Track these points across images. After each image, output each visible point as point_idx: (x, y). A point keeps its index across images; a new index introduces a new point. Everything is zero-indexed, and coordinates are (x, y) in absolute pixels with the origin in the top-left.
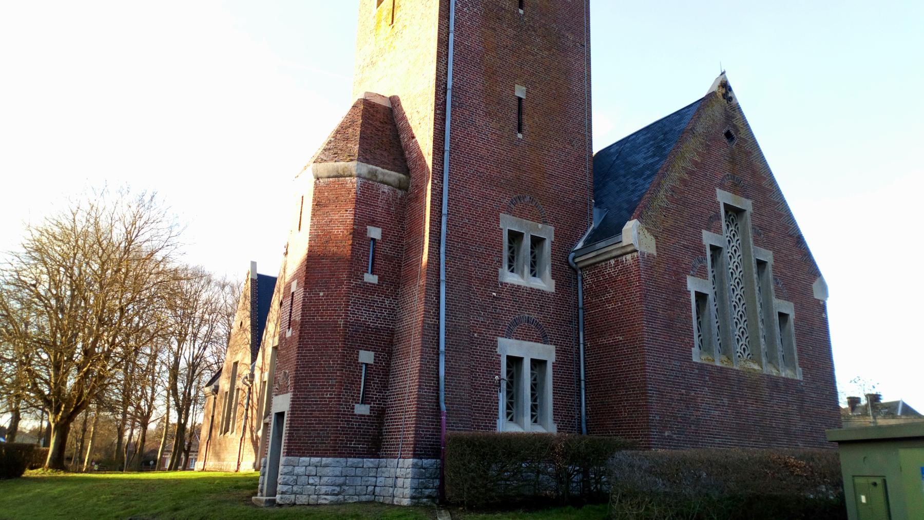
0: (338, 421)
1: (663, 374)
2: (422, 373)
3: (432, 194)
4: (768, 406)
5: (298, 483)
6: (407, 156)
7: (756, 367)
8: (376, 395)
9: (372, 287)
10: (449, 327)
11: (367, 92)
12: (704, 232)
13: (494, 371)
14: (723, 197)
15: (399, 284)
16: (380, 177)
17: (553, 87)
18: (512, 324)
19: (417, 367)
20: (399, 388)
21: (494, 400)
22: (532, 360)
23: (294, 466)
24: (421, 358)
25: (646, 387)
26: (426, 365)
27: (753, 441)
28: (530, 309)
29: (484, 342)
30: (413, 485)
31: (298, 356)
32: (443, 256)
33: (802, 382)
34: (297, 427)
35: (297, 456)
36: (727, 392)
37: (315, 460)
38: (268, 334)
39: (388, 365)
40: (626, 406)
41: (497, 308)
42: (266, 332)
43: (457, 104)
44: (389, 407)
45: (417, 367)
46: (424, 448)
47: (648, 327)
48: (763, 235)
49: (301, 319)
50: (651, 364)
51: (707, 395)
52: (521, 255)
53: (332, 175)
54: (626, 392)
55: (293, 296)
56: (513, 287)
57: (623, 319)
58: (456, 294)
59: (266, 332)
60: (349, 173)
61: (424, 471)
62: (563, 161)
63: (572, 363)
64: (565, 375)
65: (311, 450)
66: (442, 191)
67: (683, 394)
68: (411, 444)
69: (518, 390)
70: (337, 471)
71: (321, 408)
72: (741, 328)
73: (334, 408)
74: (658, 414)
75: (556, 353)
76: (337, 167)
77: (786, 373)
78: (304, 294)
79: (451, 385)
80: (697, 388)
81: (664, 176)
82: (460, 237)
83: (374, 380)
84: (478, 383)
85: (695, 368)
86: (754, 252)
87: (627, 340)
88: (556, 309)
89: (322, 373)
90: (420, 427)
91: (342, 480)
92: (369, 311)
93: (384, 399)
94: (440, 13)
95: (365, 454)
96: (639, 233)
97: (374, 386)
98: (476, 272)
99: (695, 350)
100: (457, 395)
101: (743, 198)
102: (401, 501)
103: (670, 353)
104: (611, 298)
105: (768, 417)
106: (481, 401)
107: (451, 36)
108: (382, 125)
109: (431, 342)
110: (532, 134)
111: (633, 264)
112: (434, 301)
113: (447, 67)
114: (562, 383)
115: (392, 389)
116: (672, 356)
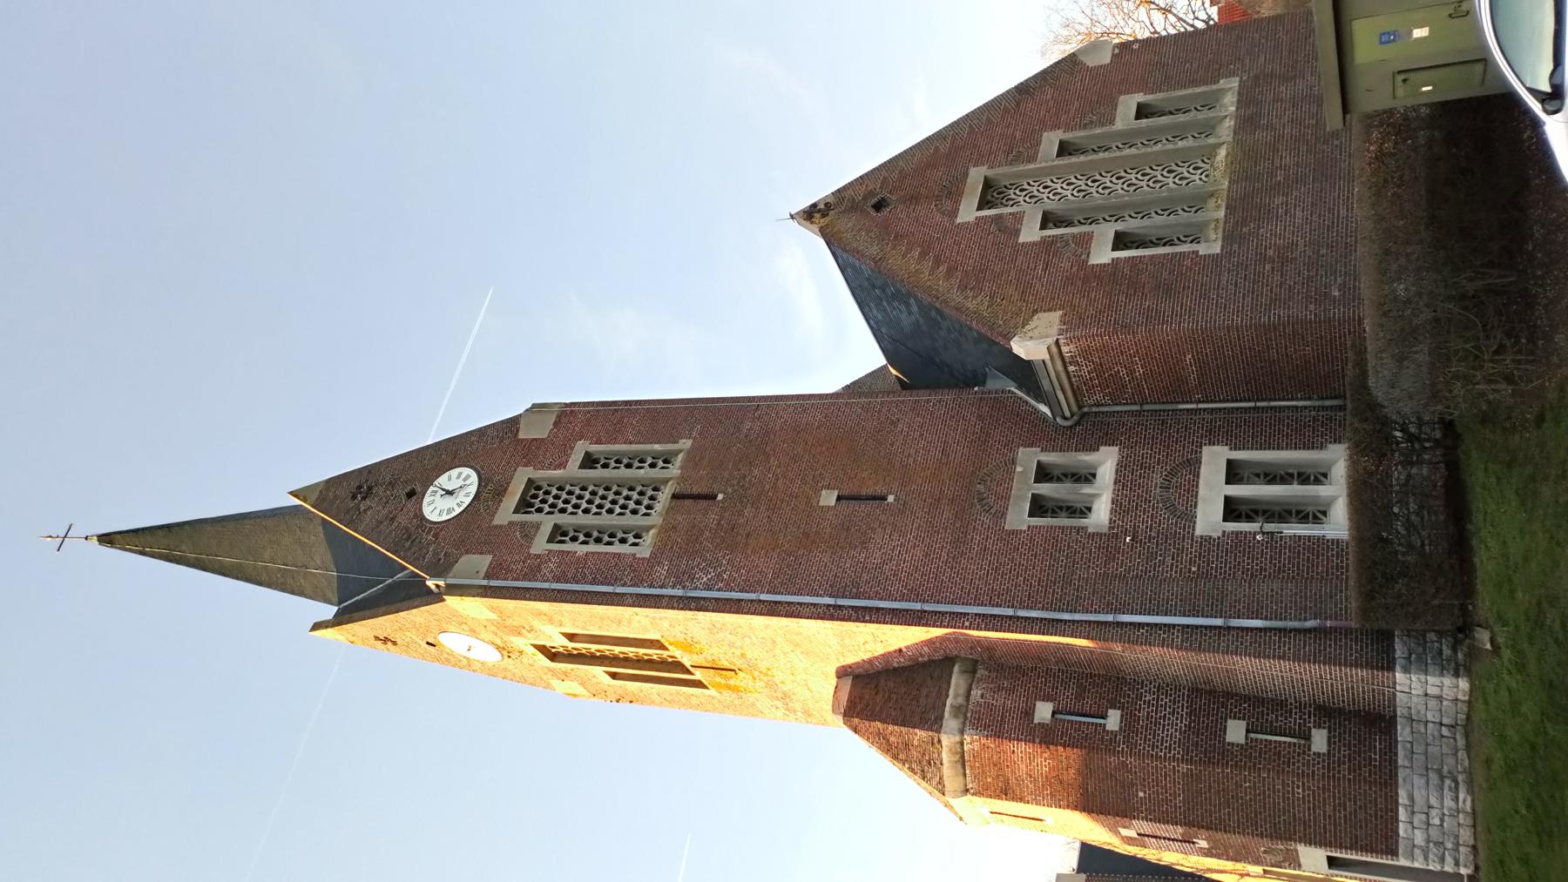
0: (1339, 778)
1: (1244, 299)
2: (1260, 653)
3: (985, 630)
4: (1284, 132)
5: (1441, 840)
6: (926, 659)
7: (1222, 152)
8: (1295, 719)
9: (1126, 719)
10: (1185, 611)
11: (833, 711)
12: (1021, 240)
13: (1250, 542)
14: (968, 212)
15: (1118, 678)
16: (961, 700)
17: (818, 451)
18: (1173, 513)
19: (1251, 661)
20: (1284, 685)
21: (1295, 542)
22: (1228, 482)
23: (1414, 846)
24: (1236, 654)
25: (1264, 324)
26: (1246, 646)
27: (1341, 154)
28: (1147, 484)
29: (1204, 556)
30: (1437, 673)
31: (1239, 833)
32: (1077, 617)
33: (1241, 78)
34: (1351, 839)
35: (1397, 842)
36: (1265, 197)
37: (1402, 814)
38: (1181, 862)
39: (1247, 698)
40: (1295, 349)
41: (1150, 535)
42: (1178, 865)
43: (854, 590)
44: (1314, 700)
45: (1251, 661)
46: (1378, 655)
47: (1171, 323)
48: (1024, 149)
49: (1181, 826)
50: (1228, 317)
51: (1271, 230)
52: (1066, 497)
53: (962, 771)
54: (1273, 348)
55: (1144, 835)
56: (1116, 511)
57: (1159, 355)
58: (1133, 597)
59: (1178, 865)
60: (959, 745)
61: (1414, 656)
62: (922, 435)
63: (1228, 421)
64: (1249, 432)
65: (1387, 820)
66: (980, 615)
67: (1273, 268)
68: (1373, 673)
69: (1277, 504)
70: (1419, 782)
71: (1319, 802)
72: (1162, 175)
73: (1318, 783)
74: (1306, 307)
75: (1214, 444)
76: (950, 762)
77: (1229, 103)
78: (1142, 820)
79: (1276, 610)
80: (1262, 245)
81: (945, 301)
82: (1046, 591)
83: (1272, 722)
84: (1270, 568)
85: (1231, 249)
86: (1047, 162)
87: (1192, 349)
88: (1144, 446)
89: (1264, 799)
90: (1346, 660)
91: (1433, 776)
92: (1164, 725)
93: (1301, 706)
94: (733, 613)
95: (1390, 738)
96: (1031, 337)
97: (1281, 721)
98: (1097, 566)
99: (1203, 249)
100: (1291, 602)
101: (968, 180)
102: (1463, 691)
103: (1210, 288)
104: (1126, 369)
105: (1300, 130)
106: (1298, 563)
107: (764, 597)
108: (881, 692)
109: (1210, 637)
110: (887, 481)
111: (1076, 343)
112: (1147, 631)
113: (805, 604)
114: (1261, 435)
115: (1285, 695)
116: (1214, 284)
